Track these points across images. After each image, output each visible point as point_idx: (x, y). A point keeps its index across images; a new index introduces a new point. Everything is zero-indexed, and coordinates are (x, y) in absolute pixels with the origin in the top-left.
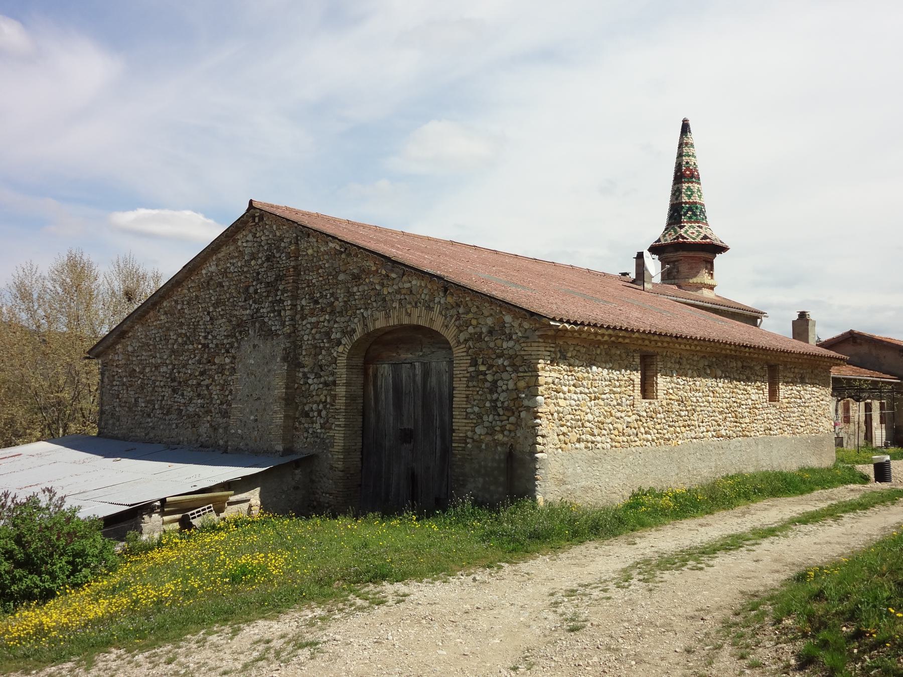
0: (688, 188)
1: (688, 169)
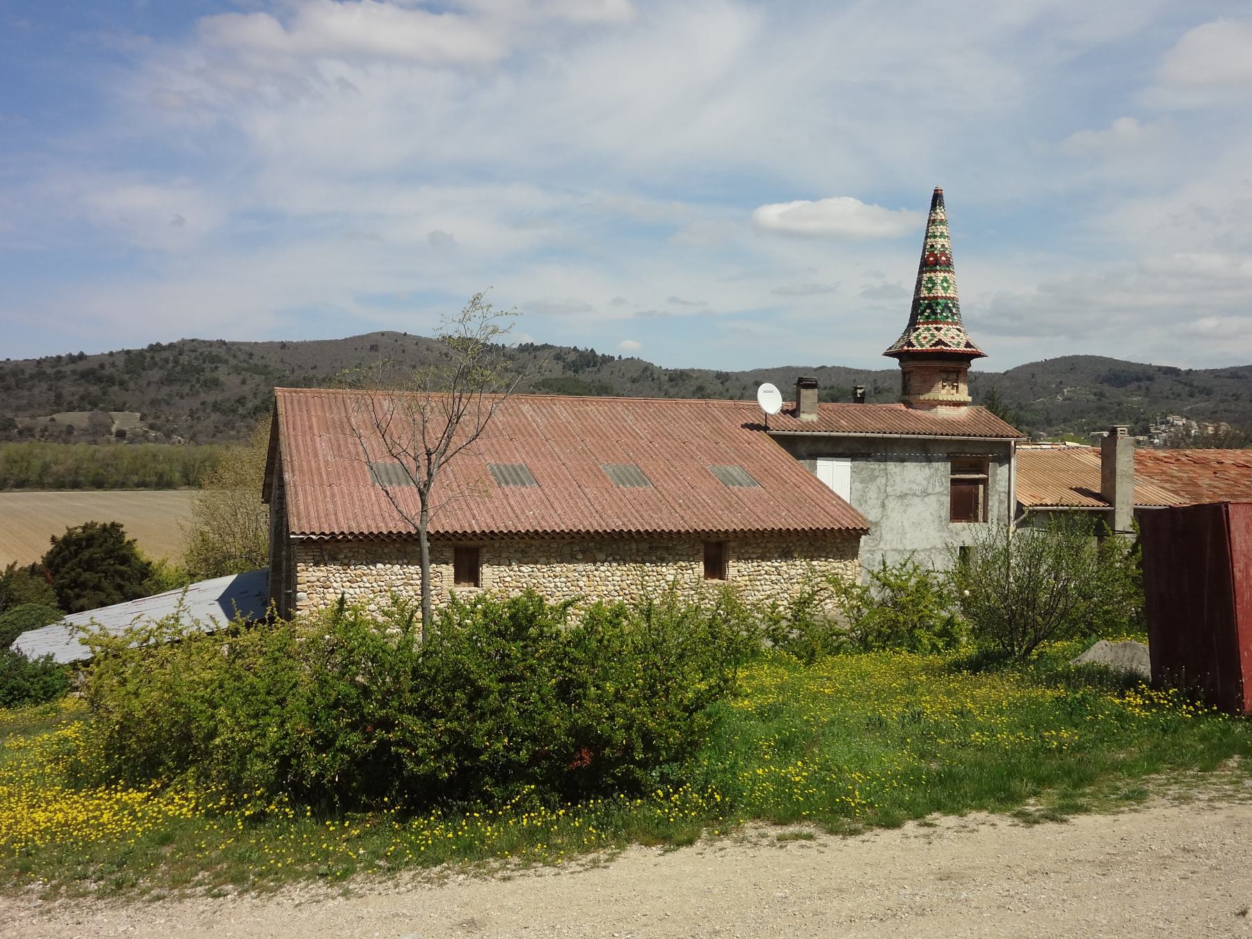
0: (945, 280)
1: (943, 253)
